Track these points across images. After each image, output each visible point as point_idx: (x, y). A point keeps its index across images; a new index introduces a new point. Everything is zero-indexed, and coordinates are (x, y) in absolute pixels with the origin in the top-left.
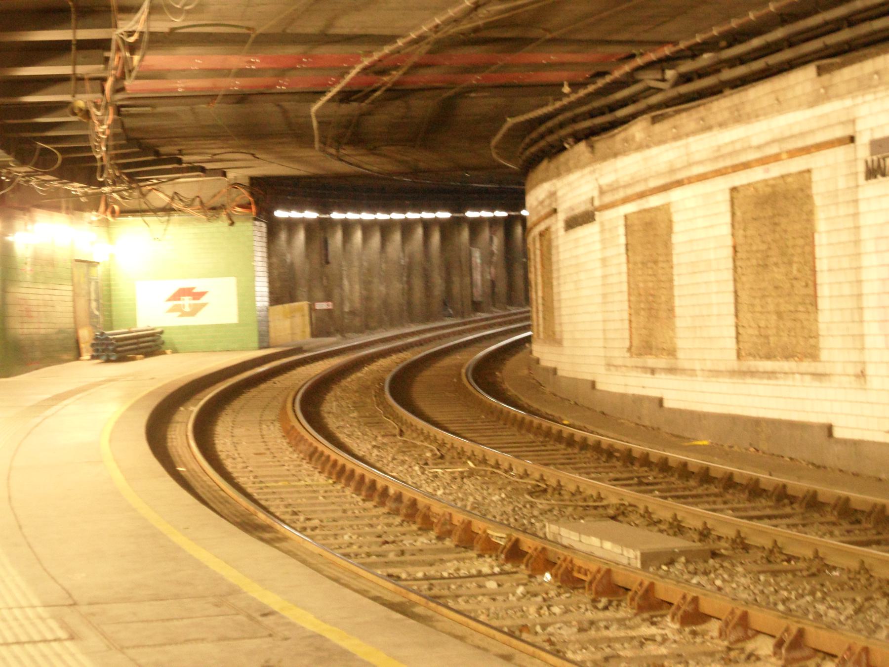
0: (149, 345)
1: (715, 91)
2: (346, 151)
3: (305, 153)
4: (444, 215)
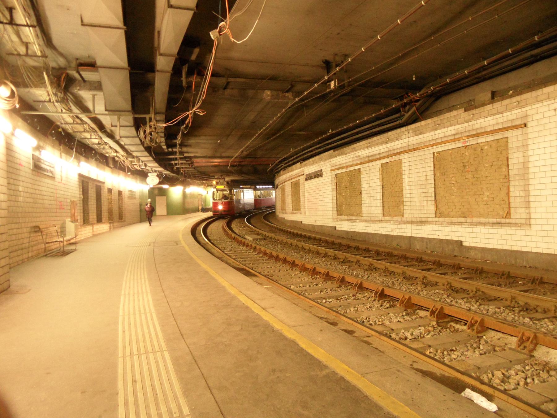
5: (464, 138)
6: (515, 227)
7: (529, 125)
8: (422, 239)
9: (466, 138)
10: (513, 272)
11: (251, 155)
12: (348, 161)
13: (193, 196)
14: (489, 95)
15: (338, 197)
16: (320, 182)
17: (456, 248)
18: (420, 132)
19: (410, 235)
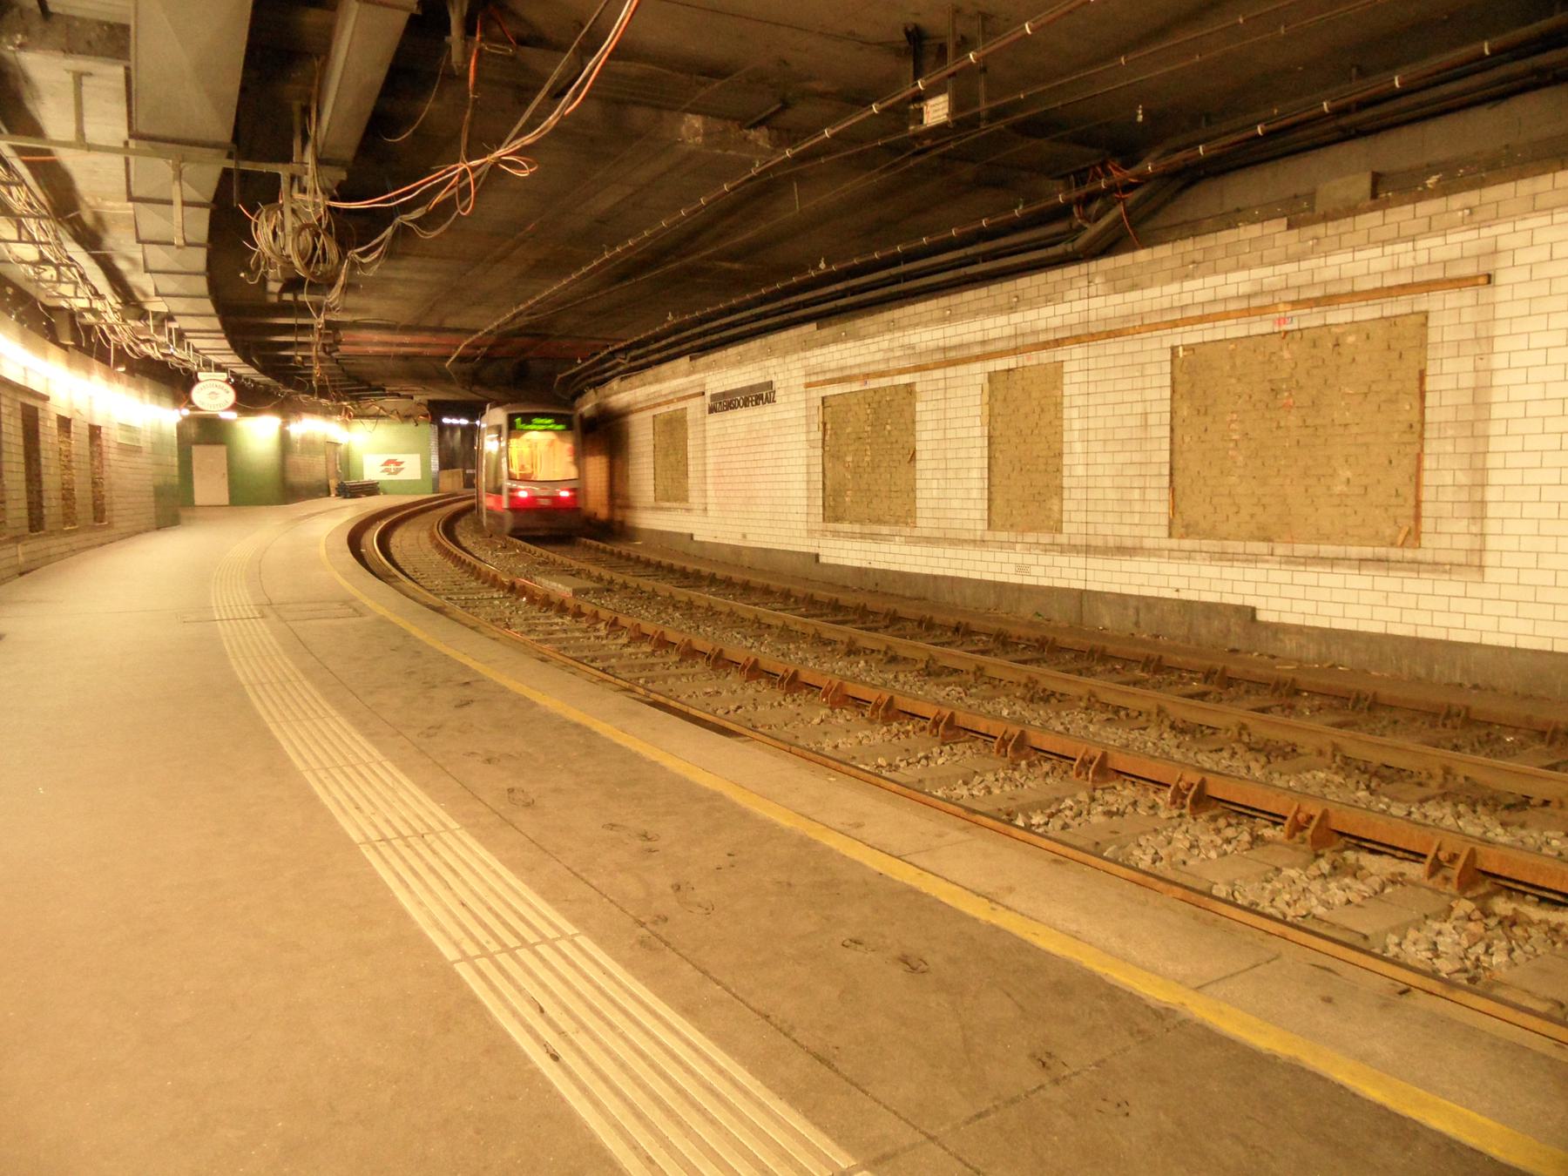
0: (371, 489)
1: (649, 366)
2: (476, 388)
3: (453, 388)
4: (464, 422)
5: (1281, 307)
6: (1433, 571)
7: (1500, 278)
8: (1122, 599)
9: (1289, 307)
10: (1479, 704)
11: (536, 331)
12: (869, 358)
13: (309, 445)
14: (1365, 184)
15: (829, 465)
16: (766, 418)
17: (1236, 629)
18: (1128, 282)
19: (1080, 585)
